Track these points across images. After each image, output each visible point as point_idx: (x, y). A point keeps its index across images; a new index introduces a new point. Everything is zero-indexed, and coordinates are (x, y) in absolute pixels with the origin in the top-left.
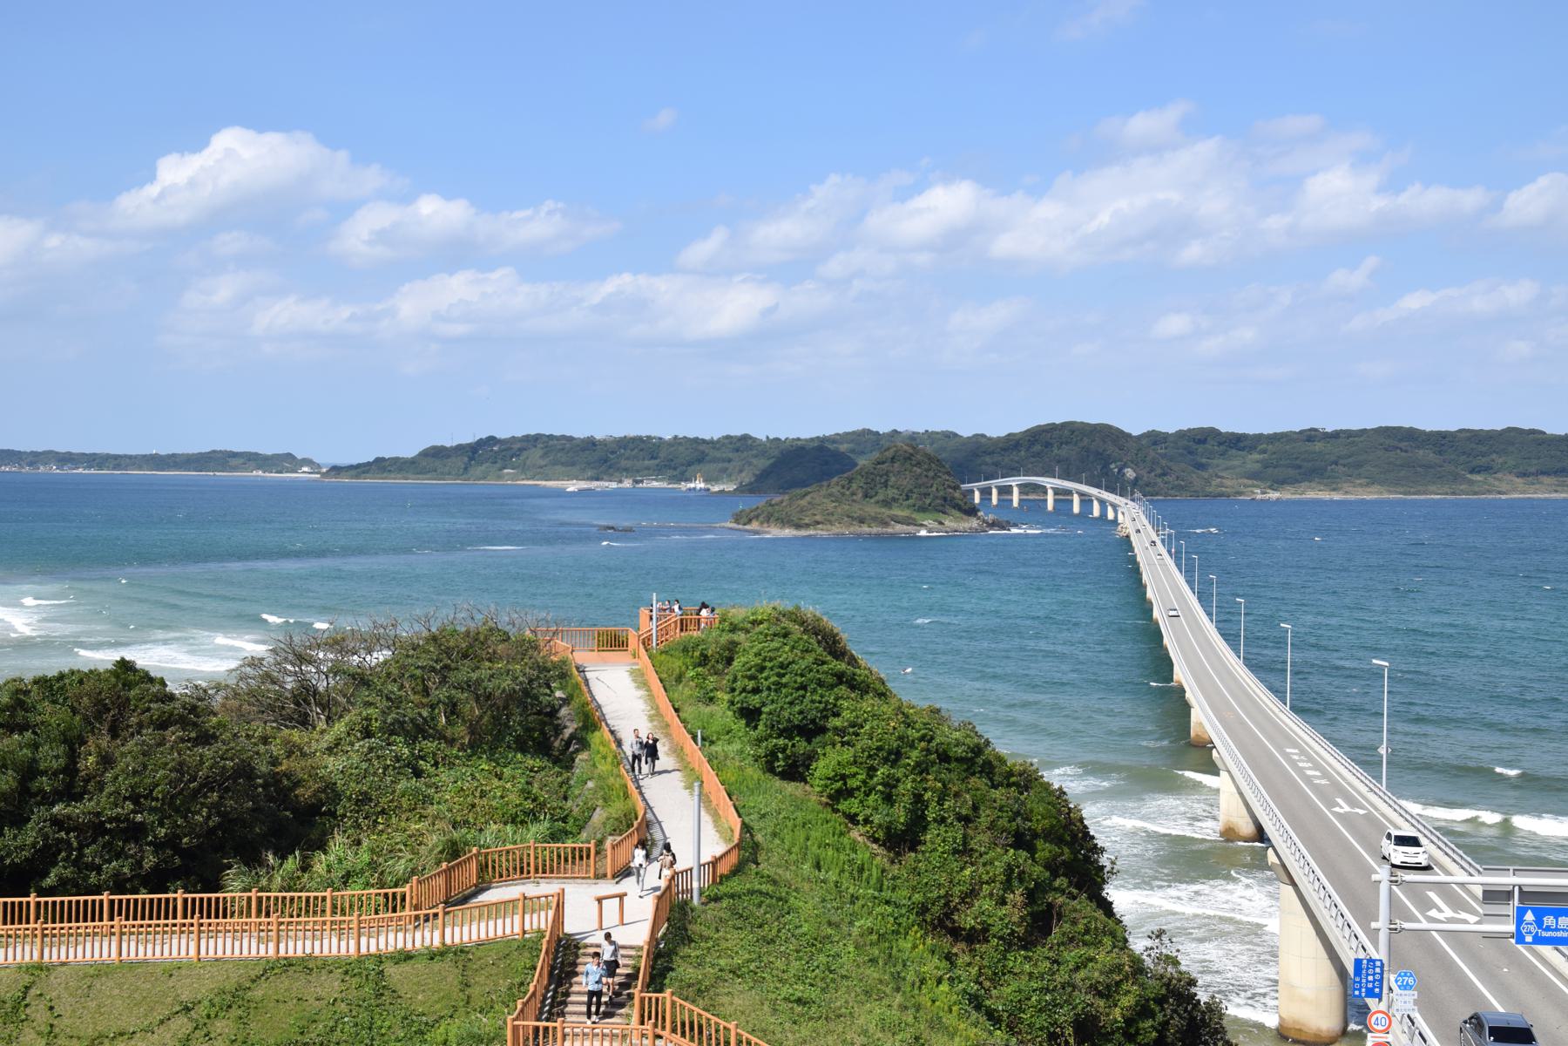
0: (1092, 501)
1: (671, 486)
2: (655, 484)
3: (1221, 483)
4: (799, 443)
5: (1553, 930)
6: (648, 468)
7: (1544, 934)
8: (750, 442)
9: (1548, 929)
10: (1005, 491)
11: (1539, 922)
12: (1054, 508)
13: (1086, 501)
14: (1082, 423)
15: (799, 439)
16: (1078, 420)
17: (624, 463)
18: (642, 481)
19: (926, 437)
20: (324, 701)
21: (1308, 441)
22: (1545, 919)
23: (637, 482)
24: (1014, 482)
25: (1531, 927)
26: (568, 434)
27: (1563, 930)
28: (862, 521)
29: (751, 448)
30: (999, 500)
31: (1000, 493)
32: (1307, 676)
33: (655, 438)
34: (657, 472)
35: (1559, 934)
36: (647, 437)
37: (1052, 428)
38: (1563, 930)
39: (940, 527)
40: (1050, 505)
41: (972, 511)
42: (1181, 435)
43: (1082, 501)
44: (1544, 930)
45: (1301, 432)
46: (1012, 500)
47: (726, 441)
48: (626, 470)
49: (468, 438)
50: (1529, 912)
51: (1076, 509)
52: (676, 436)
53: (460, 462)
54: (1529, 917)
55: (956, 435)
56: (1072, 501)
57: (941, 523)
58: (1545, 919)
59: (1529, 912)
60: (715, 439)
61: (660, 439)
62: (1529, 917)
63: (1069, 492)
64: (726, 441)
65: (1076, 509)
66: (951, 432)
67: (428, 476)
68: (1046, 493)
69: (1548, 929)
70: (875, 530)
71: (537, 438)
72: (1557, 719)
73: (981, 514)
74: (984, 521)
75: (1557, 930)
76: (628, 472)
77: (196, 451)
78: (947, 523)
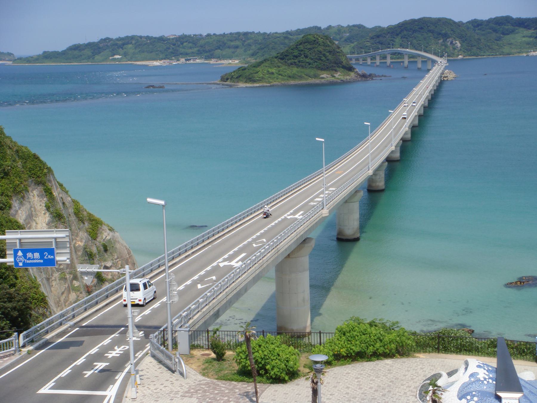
5: (32, 259)
7: (28, 262)
9: (29, 259)
11: (25, 256)
15: (276, 33)
17: (182, 50)
18: (190, 59)
20: (17, 189)
22: (27, 254)
25: (21, 259)
26: (104, 37)
27: (37, 259)
34: (199, 54)
35: (35, 261)
36: (194, 35)
38: (37, 259)
42: (489, 21)
44: (27, 260)
48: (181, 54)
49: (95, 38)
50: (20, 251)
52: (349, 25)
53: (88, 52)
54: (20, 253)
57: (334, 76)
58: (27, 254)
59: (20, 251)
61: (201, 35)
62: (20, 253)
67: (7, 64)
69: (29, 259)
71: (133, 37)
75: (34, 259)
76: (185, 54)
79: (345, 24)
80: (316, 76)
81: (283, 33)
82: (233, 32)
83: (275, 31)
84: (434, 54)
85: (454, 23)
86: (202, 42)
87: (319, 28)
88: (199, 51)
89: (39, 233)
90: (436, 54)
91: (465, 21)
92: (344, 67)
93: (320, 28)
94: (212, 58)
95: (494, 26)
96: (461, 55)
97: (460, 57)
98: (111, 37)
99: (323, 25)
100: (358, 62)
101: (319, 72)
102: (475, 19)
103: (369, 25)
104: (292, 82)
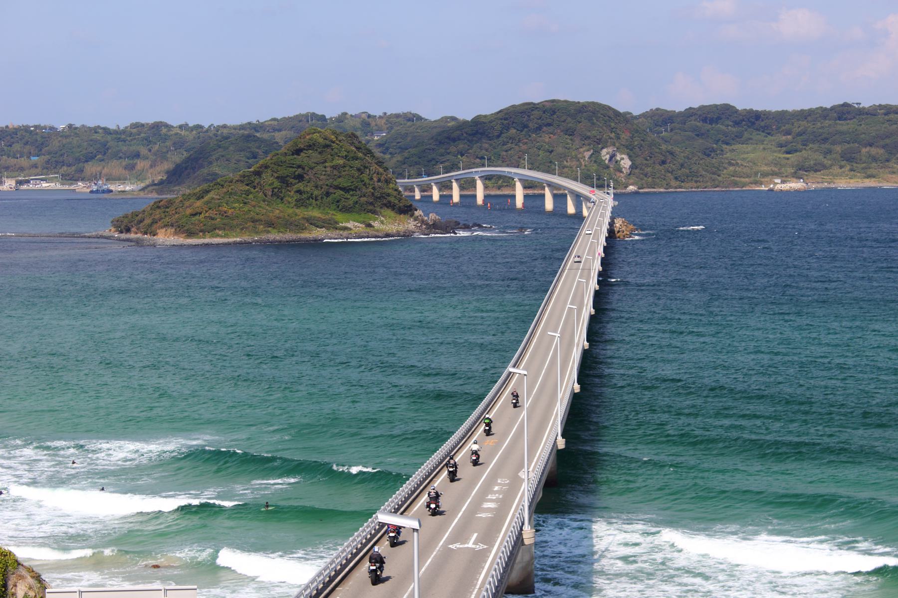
0: (565, 196)
1: (66, 187)
2: (45, 185)
3: (735, 171)
4: (225, 131)
6: (35, 166)
8: (164, 130)
10: (468, 184)
12: (555, 207)
13: (560, 198)
14: (566, 101)
15: (225, 126)
16: (562, 98)
19: (384, 121)
21: (840, 119)
23: (20, 183)
24: (477, 173)
26: (149, 118)
28: (271, 224)
29: (165, 138)
30: (461, 196)
31: (462, 188)
32: (874, 395)
33: (45, 128)
34: (51, 167)
36: (36, 127)
37: (529, 109)
39: (368, 230)
40: (519, 202)
41: (407, 210)
42: (690, 113)
43: (555, 196)
45: (833, 108)
46: (475, 196)
47: (134, 131)
51: (549, 205)
55: (419, 118)
56: (543, 196)
57: (369, 226)
60: (122, 128)
61: (52, 128)
63: (539, 185)
64: (134, 131)
65: (549, 205)
66: (414, 115)
68: (513, 187)
70: (289, 236)
72: (895, 463)
73: (418, 213)
74: (423, 222)
77: (798, 108)
78: (376, 224)
79: (377, 112)
80: (331, 225)
81: (242, 127)
82: (143, 121)
83: (221, 123)
84: (581, 182)
85: (617, 114)
86: (55, 144)
87: (323, 118)
88: (48, 162)
89: (415, 503)
90: (586, 179)
91: (636, 113)
92: (390, 206)
93: (324, 116)
94: (77, 180)
95: (699, 124)
96: (632, 184)
97: (631, 188)
98: (423, 115)
99: (331, 112)
100: (412, 194)
101: (339, 216)
102: (657, 109)
103: (740, 107)
104: (274, 235)
